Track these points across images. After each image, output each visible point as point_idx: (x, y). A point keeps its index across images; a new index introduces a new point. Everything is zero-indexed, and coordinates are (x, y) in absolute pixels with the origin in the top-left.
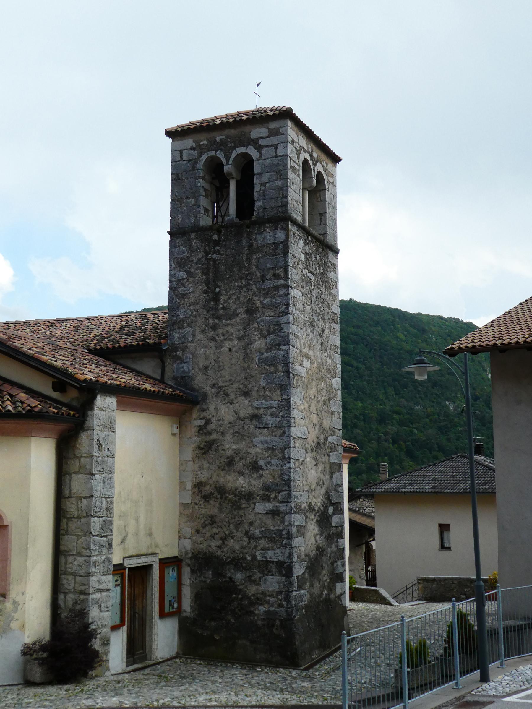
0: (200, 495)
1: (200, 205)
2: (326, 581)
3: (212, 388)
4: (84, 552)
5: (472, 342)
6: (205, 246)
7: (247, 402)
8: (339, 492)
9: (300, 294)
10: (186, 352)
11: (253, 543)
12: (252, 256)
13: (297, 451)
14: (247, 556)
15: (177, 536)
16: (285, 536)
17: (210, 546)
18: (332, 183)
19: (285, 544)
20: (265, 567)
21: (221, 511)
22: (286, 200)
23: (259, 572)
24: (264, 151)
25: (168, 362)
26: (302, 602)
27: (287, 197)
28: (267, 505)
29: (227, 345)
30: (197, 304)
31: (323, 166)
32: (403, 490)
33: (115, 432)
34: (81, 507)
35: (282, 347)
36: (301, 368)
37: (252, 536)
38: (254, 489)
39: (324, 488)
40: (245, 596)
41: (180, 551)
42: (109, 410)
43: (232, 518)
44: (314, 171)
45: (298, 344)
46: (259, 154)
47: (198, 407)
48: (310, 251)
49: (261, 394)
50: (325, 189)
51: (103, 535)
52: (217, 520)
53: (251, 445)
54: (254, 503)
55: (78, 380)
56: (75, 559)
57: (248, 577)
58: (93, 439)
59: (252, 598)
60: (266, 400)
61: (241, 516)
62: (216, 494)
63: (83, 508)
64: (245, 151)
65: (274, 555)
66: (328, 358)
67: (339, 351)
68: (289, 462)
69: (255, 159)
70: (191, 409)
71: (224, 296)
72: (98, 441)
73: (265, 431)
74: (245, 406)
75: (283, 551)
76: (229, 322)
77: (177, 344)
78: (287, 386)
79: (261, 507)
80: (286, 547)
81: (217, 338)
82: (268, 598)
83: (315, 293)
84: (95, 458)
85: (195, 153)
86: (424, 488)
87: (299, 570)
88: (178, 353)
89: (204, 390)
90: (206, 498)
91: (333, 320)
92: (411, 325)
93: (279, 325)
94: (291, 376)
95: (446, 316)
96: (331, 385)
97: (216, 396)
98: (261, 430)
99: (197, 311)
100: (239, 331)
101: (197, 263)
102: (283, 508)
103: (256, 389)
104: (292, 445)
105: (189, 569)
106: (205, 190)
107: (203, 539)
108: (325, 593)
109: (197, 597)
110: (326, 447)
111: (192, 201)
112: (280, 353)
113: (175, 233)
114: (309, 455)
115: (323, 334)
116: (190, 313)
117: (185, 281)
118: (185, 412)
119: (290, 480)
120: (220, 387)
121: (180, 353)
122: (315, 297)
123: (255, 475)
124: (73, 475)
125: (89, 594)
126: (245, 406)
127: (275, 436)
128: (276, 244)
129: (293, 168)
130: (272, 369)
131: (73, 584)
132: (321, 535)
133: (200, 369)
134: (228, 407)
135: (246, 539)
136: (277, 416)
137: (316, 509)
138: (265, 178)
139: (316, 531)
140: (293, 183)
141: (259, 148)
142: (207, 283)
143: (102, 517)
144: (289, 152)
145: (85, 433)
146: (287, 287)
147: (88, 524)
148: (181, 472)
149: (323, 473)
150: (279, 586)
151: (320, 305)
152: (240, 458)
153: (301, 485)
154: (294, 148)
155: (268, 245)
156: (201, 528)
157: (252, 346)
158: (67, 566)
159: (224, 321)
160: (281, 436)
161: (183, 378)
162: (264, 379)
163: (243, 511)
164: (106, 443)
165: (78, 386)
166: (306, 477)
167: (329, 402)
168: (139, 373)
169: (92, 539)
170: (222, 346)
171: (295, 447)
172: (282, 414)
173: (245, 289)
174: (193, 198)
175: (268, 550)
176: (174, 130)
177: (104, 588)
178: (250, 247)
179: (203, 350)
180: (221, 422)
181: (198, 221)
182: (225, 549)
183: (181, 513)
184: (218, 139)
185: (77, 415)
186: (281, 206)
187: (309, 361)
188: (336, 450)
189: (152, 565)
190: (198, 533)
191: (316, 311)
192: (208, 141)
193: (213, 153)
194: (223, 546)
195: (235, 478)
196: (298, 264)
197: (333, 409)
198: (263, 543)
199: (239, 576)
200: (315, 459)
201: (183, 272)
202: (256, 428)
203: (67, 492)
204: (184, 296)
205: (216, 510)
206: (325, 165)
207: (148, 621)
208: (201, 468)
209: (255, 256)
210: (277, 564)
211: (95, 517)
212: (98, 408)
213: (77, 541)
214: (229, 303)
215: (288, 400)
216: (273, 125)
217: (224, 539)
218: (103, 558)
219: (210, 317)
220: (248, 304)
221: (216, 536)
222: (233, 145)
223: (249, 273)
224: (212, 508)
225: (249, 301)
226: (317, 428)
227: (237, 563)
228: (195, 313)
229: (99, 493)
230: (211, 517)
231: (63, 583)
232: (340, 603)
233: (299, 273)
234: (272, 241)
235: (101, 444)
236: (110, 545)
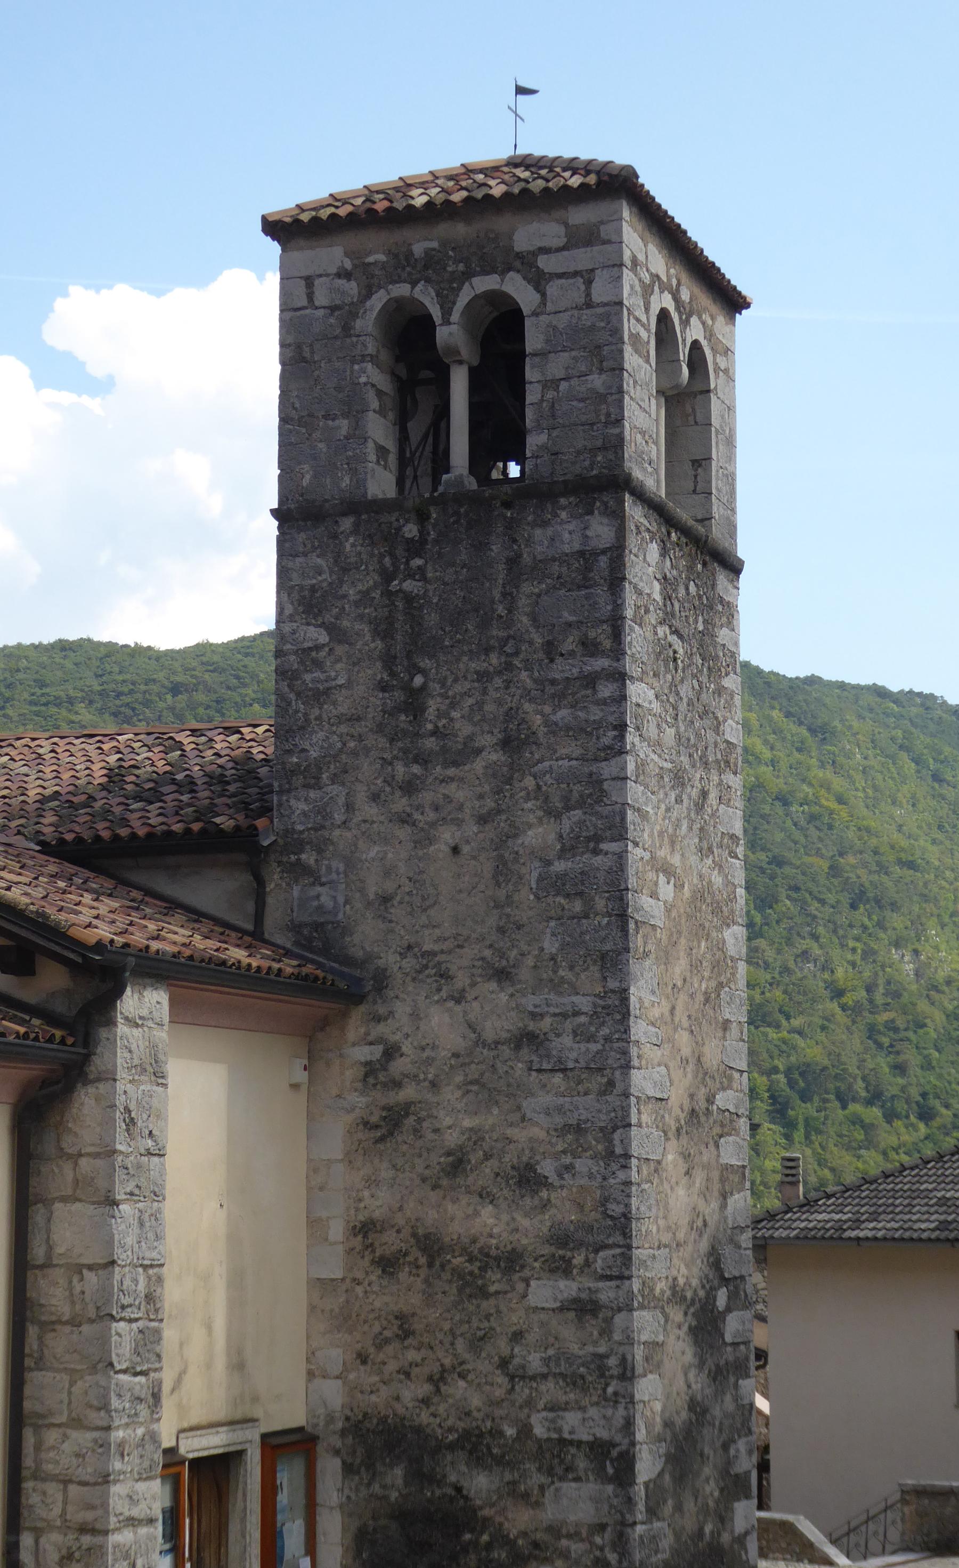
0: (368, 1258)
1: (366, 440)
2: (712, 1495)
3: (403, 956)
4: (94, 1417)
6: (382, 556)
7: (503, 997)
8: (740, 1247)
9: (651, 694)
10: (328, 854)
11: (523, 1392)
12: (517, 587)
13: (646, 1138)
14: (506, 1428)
15: (304, 1372)
16: (615, 1372)
17: (398, 1398)
18: (726, 371)
19: (616, 1394)
20: (557, 1457)
21: (429, 1300)
22: (616, 431)
23: (539, 1469)
24: (553, 289)
25: (275, 880)
26: (656, 1552)
27: (619, 421)
28: (562, 1284)
29: (447, 835)
30: (359, 719)
31: (704, 323)
32: (853, 1234)
33: (165, 1086)
34: (83, 1293)
35: (604, 846)
36: (654, 902)
37: (521, 1372)
38: (524, 1241)
39: (705, 1237)
41: (311, 1412)
42: (150, 1023)
43: (461, 1322)
44: (684, 340)
45: (646, 835)
46: (537, 297)
47: (362, 1008)
48: (675, 572)
49: (545, 976)
50: (709, 391)
51: (138, 1369)
52: (418, 1326)
53: (515, 1117)
54: (527, 1281)
55: (77, 944)
56: (65, 1437)
57: (508, 1483)
58: (113, 1106)
59: (520, 1542)
60: (560, 994)
61: (488, 1317)
62: (415, 1253)
63: (88, 1297)
64: (497, 287)
65: (583, 1424)
66: (716, 872)
67: (740, 851)
68: (625, 1167)
69: (526, 311)
70: (345, 1015)
71: (439, 700)
72: (128, 1110)
73: (558, 1079)
74: (497, 1011)
75: (609, 1412)
76: (451, 772)
77: (301, 832)
78: (620, 954)
79: (545, 1292)
80: (616, 1402)
81: (417, 816)
82: (564, 1542)
84: (120, 1158)
85: (352, 288)
86: (916, 1226)
87: (647, 1466)
88: (303, 856)
89: (381, 963)
90: (388, 1265)
91: (727, 763)
92: (788, 715)
93: (596, 782)
94: (632, 926)
95: (894, 688)
96: (721, 946)
97: (414, 979)
98: (544, 1077)
99: (360, 738)
101: (357, 604)
102: (607, 1293)
103: (530, 961)
104: (634, 1121)
105: (337, 1463)
106: (380, 393)
107: (377, 1378)
108: (708, 1529)
110: (711, 1121)
111: (343, 425)
112: (598, 860)
113: (292, 516)
114: (673, 1144)
115: (703, 806)
116: (339, 745)
117: (323, 654)
118: (324, 1024)
119: (627, 1216)
121: (309, 858)
122: (685, 700)
123: (528, 1201)
124: (58, 1205)
125: (106, 1533)
126: (497, 1011)
127: (586, 1094)
128: (587, 557)
129: (635, 337)
130: (578, 906)
131: (60, 1504)
132: (701, 1365)
134: (449, 1010)
135: (501, 1379)
136: (591, 1038)
137: (689, 1295)
138: (557, 366)
139: (689, 1357)
140: (635, 382)
141: (539, 280)
142: (389, 660)
143: (137, 1320)
144: (625, 295)
145: (91, 1089)
146: (621, 677)
147: (104, 1341)
148: (315, 1190)
149: (703, 1194)
150: (597, 1509)
151: (697, 725)
152: (485, 1154)
153: (654, 1230)
154: (637, 282)
155: (563, 559)
156: (372, 1350)
157: (520, 841)
158: (43, 1455)
159: (438, 768)
160: (602, 1093)
162: (553, 934)
163: (492, 1301)
164: (145, 1116)
165: (80, 960)
166: (667, 1204)
167: (719, 995)
168: (195, 915)
169: (113, 1382)
170: (431, 841)
171: (639, 1125)
172: (605, 1031)
173: (498, 681)
174: (346, 415)
175: (565, 1410)
176: (288, 220)
177: (142, 1516)
178: (513, 562)
179: (377, 848)
180: (428, 1052)
181: (361, 483)
182: (441, 1409)
183: (312, 1309)
184: (418, 249)
185: (70, 1040)
186: (604, 448)
187: (672, 882)
188: (734, 1131)
189: (240, 1454)
190: (364, 1362)
191: (689, 740)
192: (389, 253)
193: (402, 290)
194: (435, 1400)
195: (470, 1211)
196: (647, 611)
197: (727, 1016)
198: (550, 1390)
199: (480, 1484)
200: (686, 1156)
201: (316, 626)
202: (530, 1069)
204: (321, 695)
205: (415, 1299)
206: (710, 322)
208: (372, 1182)
209: (526, 588)
210: (591, 1449)
211: (121, 1319)
212: (126, 1019)
213: (71, 1385)
214: (452, 720)
215: (623, 995)
216: (580, 215)
217: (438, 1380)
218: (140, 1431)
219: (396, 758)
220: (506, 721)
221: (415, 1371)
222: (461, 267)
223: (509, 637)
224: (405, 1293)
226: (690, 1068)
227: (476, 1445)
228: (352, 744)
229: (129, 1253)
230: (401, 1317)
231: (31, 1501)
232: (744, 1557)
233: (649, 635)
234: (577, 546)
235: (132, 1119)
236: (156, 1397)
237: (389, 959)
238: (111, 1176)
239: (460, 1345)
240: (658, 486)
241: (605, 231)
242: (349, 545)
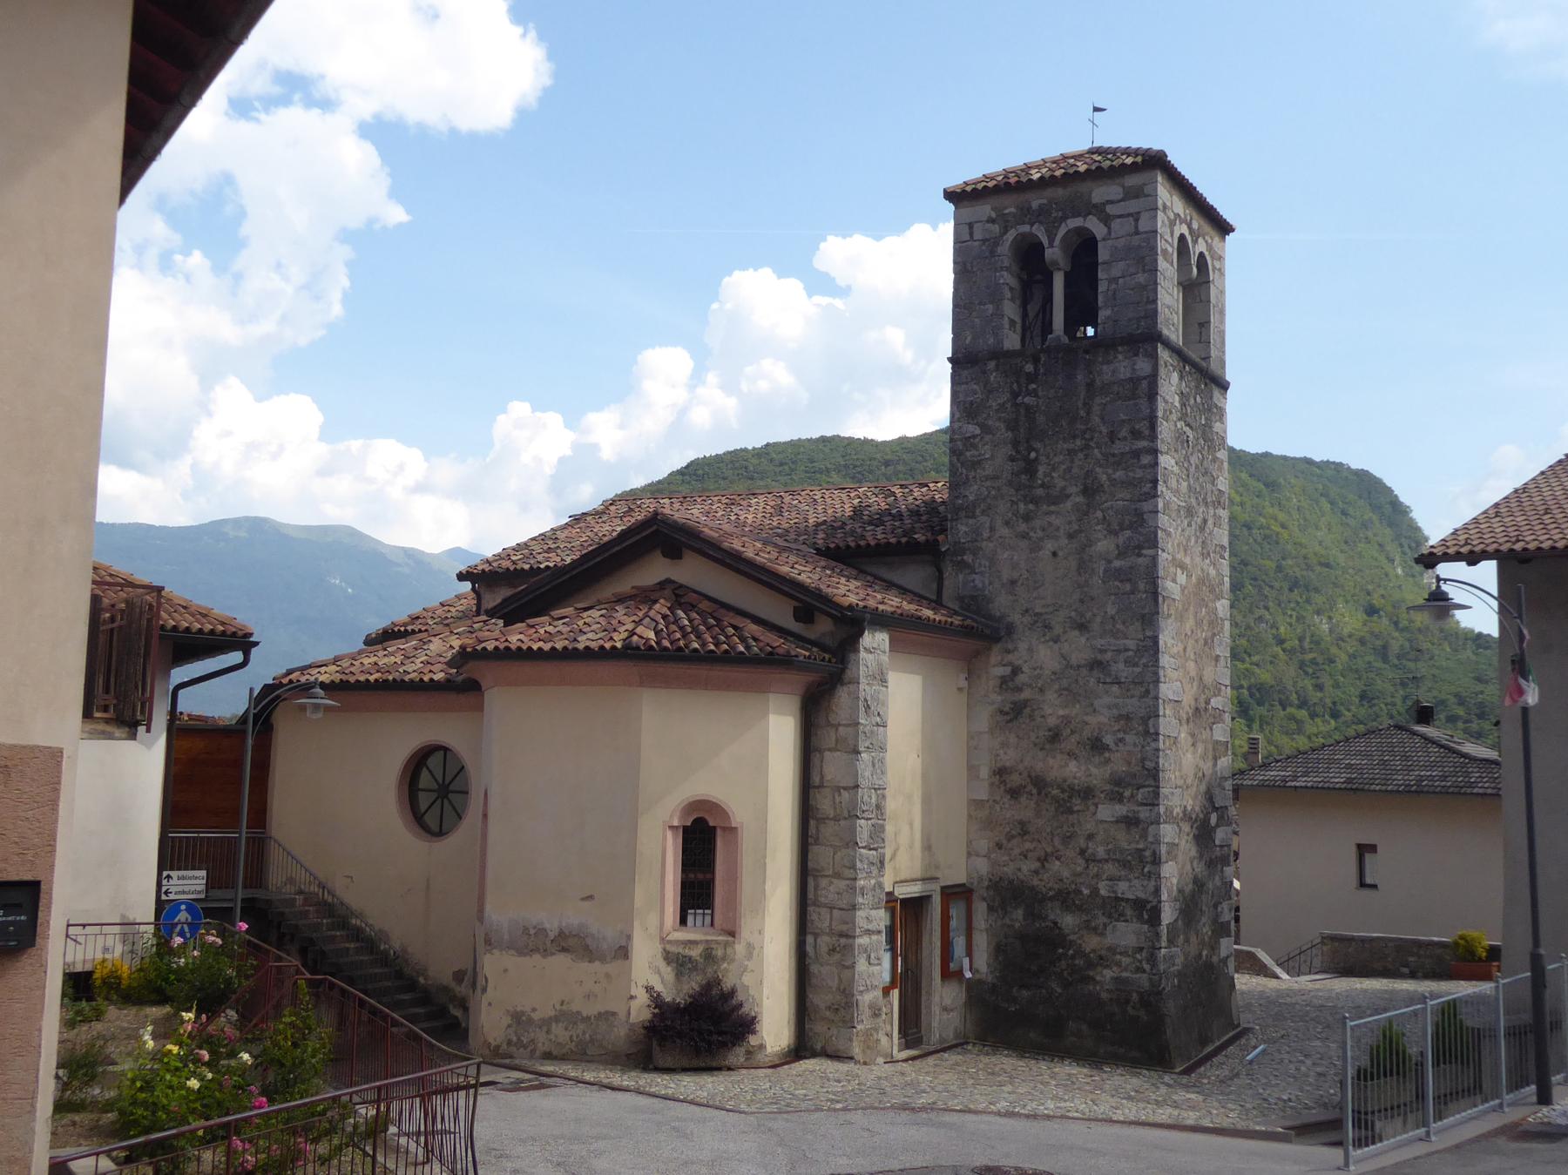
5: (1466, 544)
7: (1083, 640)
11: (1094, 869)
13: (1168, 723)
20: (1114, 907)
24: (1116, 224)
25: (949, 571)
27: (1155, 301)
28: (1117, 807)
36: (1174, 585)
40: (1080, 953)
41: (968, 875)
54: (1096, 805)
62: (1030, 787)
67: (1227, 555)
68: (1157, 740)
69: (1099, 237)
70: (989, 649)
73: (1115, 688)
74: (1078, 648)
76: (1053, 508)
79: (1107, 812)
83: (1194, 460)
85: (996, 228)
87: (1168, 915)
90: (1014, 793)
93: (1139, 515)
100: (1070, 523)
102: (1144, 813)
103: (1098, 619)
106: (1011, 289)
109: (999, 950)
111: (990, 308)
112: (1140, 560)
113: (960, 360)
118: (977, 654)
120: (1036, 614)
121: (968, 558)
123: (1097, 759)
126: (1078, 648)
128: (1135, 381)
129: (1165, 252)
130: (1128, 587)
133: (1003, 585)
135: (1080, 861)
138: (1116, 270)
139: (1194, 852)
141: (1106, 220)
142: (1015, 444)
147: (853, 830)
149: (1203, 757)
161: (973, 598)
168: (903, 591)
183: (970, 816)
184: (1035, 204)
186: (1146, 317)
189: (929, 897)
193: (1026, 228)
198: (1110, 869)
199: (1069, 921)
200: (1193, 735)
203: (816, 780)
204: (976, 464)
207: (924, 984)
208: (1004, 745)
209: (1098, 400)
216: (1132, 180)
217: (1044, 860)
224: (1025, 809)
225: (1088, 473)
227: (1066, 898)
230: (1022, 823)
236: (882, 863)
237: (1015, 618)
239: (1057, 841)
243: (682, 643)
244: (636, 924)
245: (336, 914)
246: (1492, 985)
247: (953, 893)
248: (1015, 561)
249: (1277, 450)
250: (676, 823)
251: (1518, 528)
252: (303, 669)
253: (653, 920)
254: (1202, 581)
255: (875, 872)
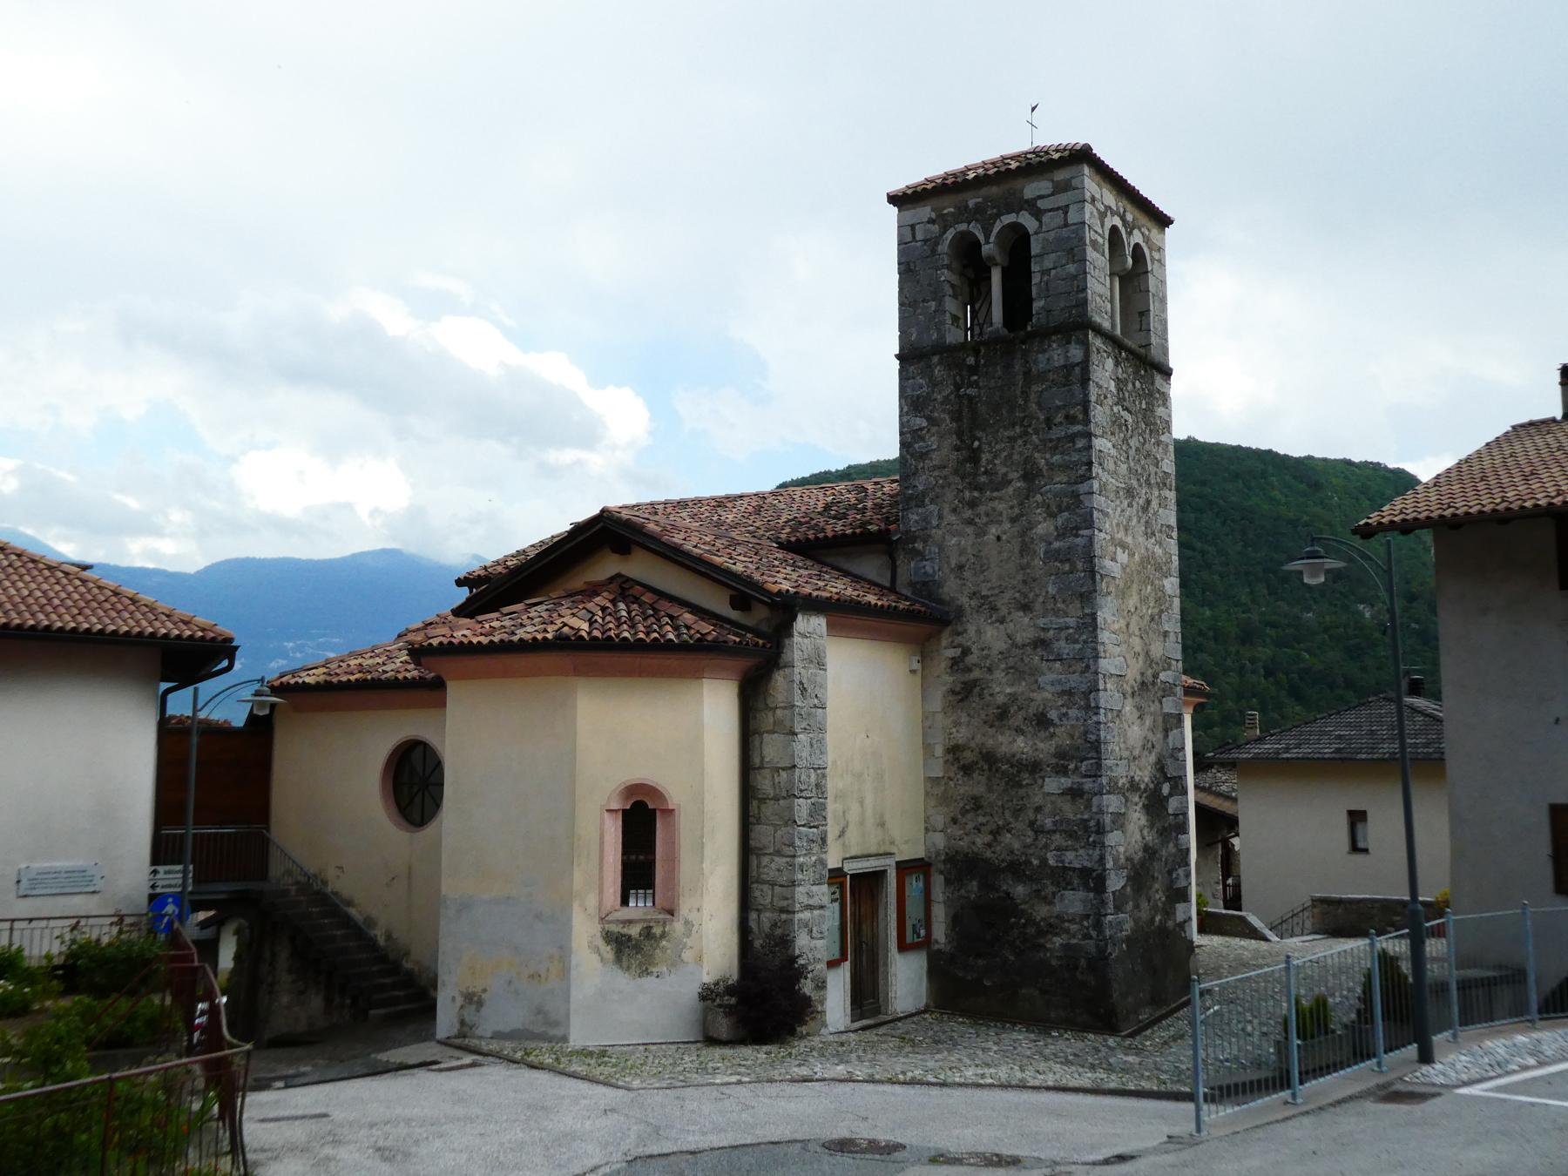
4: (786, 850)
7: (1027, 620)
9: (1110, 445)
11: (1043, 840)
13: (1109, 696)
20: (1062, 877)
21: (990, 790)
24: (1046, 218)
25: (901, 559)
27: (1085, 289)
29: (993, 530)
36: (1114, 564)
40: (1030, 921)
41: (927, 850)
53: (1034, 687)
54: (1043, 778)
62: (981, 763)
65: (1076, 858)
67: (1175, 535)
70: (940, 632)
73: (1058, 665)
74: (1024, 627)
76: (995, 494)
79: (1053, 785)
83: (1134, 443)
87: (1115, 882)
90: (967, 770)
93: (1076, 496)
96: (1162, 589)
102: (1088, 784)
103: (1041, 599)
104: (1101, 687)
106: (953, 286)
108: (1158, 919)
109: (955, 921)
112: (1078, 540)
113: (907, 357)
118: (929, 637)
119: (1098, 741)
120: (983, 597)
121: (919, 546)
123: (1042, 734)
126: (1024, 627)
128: (1068, 368)
129: (1094, 243)
130: (1067, 567)
132: (1151, 827)
133: (952, 570)
135: (1030, 833)
136: (1076, 641)
138: (1048, 262)
141: (1038, 214)
146: (1089, 435)
147: (791, 808)
160: (1083, 672)
161: (925, 584)
168: (856, 578)
173: (1020, 442)
178: (1027, 373)
183: (927, 794)
184: (971, 203)
186: (1077, 306)
193: (963, 227)
198: (1058, 839)
199: (1020, 890)
200: (1139, 708)
203: (757, 761)
204: (923, 456)
208: (957, 724)
215: (1093, 616)
216: (1061, 175)
217: (996, 833)
224: (976, 786)
226: (1141, 659)
227: (1017, 869)
230: (975, 799)
234: (1062, 362)
236: (824, 840)
237: (964, 600)
238: (792, 720)
239: (1007, 814)
240: (1113, 325)
241: (1074, 182)
242: (938, 372)
243: (612, 633)
244: (576, 906)
245: (331, 907)
246: (1367, 941)
247: (904, 868)
248: (962, 547)
249: (1318, 454)
250: (615, 806)
251: (1452, 496)
252: (294, 673)
253: (592, 901)
254: (1147, 559)
255: (816, 849)
